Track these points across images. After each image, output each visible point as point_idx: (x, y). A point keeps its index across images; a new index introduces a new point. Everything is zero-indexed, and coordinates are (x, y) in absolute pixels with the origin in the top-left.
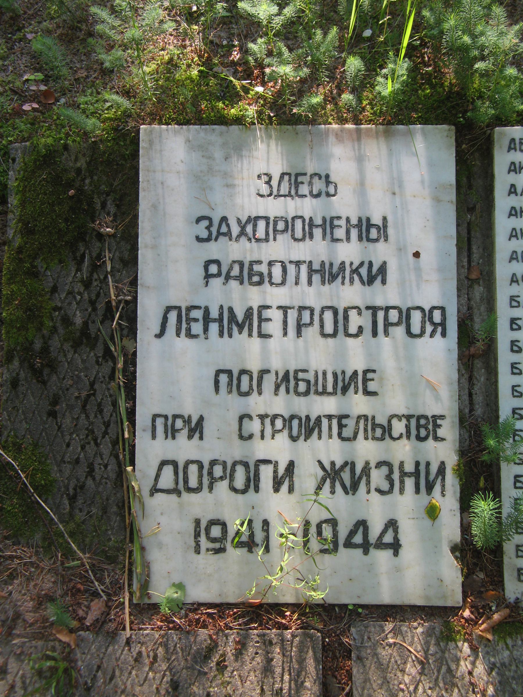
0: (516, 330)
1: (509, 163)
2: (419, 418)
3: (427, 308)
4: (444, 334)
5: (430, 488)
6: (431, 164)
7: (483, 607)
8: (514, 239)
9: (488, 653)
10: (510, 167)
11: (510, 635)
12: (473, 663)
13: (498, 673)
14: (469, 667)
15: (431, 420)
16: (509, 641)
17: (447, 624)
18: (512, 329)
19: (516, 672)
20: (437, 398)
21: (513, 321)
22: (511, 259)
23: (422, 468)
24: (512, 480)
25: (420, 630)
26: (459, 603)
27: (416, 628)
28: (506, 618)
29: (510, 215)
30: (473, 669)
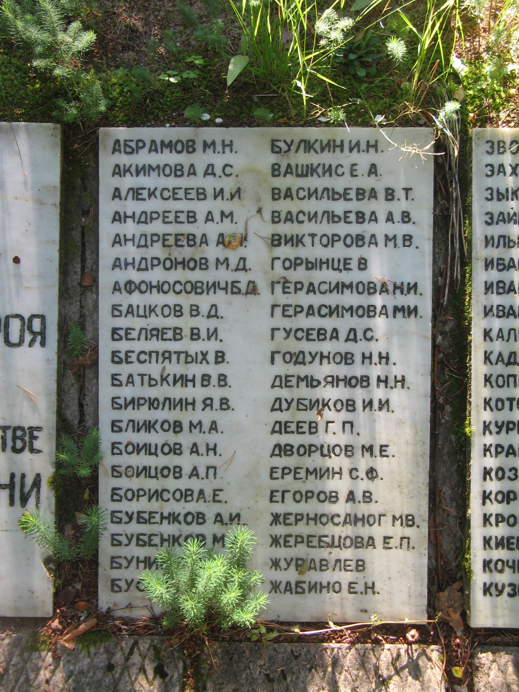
0: (117, 340)
1: (114, 166)
2: (15, 429)
3: (26, 317)
4: (43, 344)
5: (24, 500)
6: (35, 165)
7: (72, 618)
8: (117, 246)
9: (69, 661)
10: (114, 170)
11: (94, 643)
12: (53, 672)
13: (74, 681)
14: (48, 675)
15: (27, 431)
16: (92, 650)
17: (35, 635)
18: (113, 339)
19: (92, 678)
20: (35, 409)
21: (114, 331)
22: (115, 266)
23: (17, 480)
24: (110, 493)
25: (7, 641)
26: (49, 614)
27: (3, 639)
28: (93, 628)
29: (114, 220)
30: (51, 678)
